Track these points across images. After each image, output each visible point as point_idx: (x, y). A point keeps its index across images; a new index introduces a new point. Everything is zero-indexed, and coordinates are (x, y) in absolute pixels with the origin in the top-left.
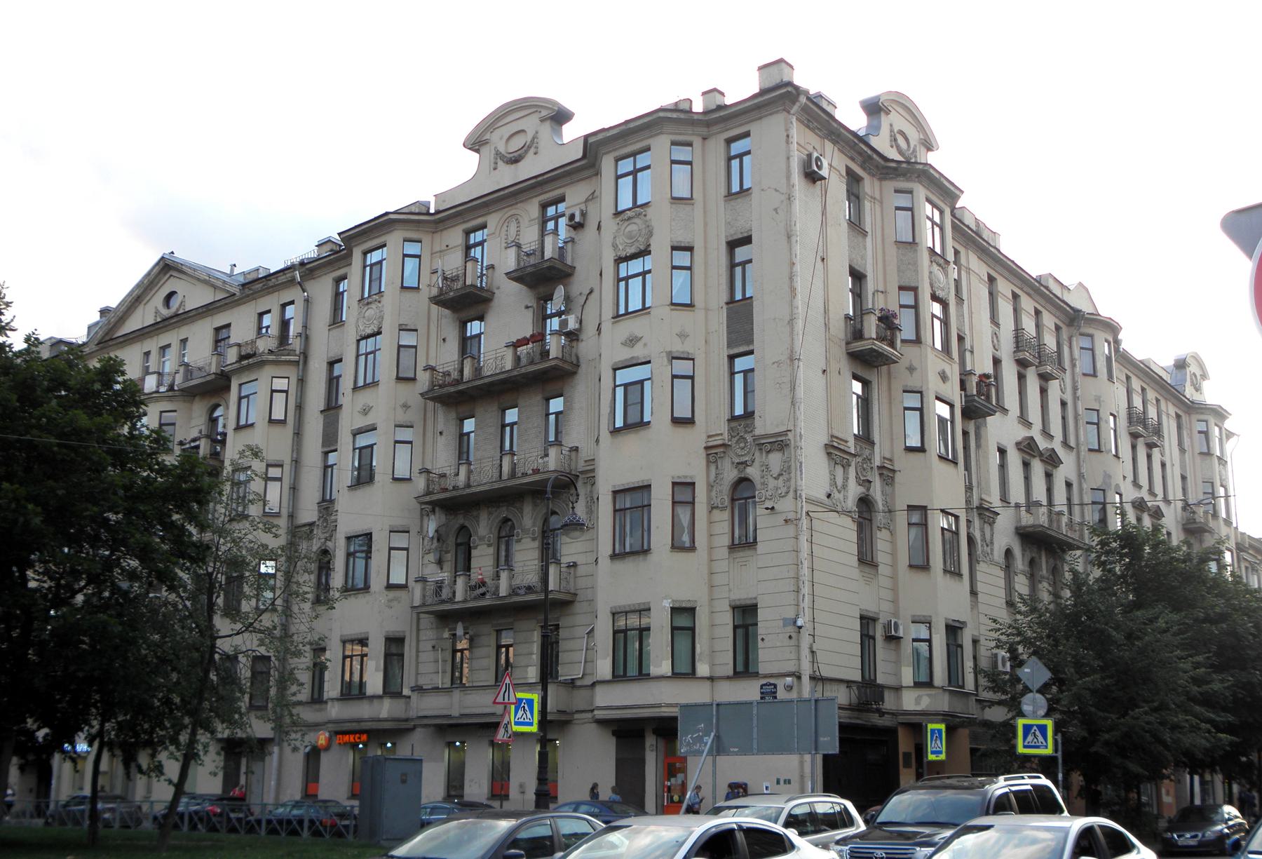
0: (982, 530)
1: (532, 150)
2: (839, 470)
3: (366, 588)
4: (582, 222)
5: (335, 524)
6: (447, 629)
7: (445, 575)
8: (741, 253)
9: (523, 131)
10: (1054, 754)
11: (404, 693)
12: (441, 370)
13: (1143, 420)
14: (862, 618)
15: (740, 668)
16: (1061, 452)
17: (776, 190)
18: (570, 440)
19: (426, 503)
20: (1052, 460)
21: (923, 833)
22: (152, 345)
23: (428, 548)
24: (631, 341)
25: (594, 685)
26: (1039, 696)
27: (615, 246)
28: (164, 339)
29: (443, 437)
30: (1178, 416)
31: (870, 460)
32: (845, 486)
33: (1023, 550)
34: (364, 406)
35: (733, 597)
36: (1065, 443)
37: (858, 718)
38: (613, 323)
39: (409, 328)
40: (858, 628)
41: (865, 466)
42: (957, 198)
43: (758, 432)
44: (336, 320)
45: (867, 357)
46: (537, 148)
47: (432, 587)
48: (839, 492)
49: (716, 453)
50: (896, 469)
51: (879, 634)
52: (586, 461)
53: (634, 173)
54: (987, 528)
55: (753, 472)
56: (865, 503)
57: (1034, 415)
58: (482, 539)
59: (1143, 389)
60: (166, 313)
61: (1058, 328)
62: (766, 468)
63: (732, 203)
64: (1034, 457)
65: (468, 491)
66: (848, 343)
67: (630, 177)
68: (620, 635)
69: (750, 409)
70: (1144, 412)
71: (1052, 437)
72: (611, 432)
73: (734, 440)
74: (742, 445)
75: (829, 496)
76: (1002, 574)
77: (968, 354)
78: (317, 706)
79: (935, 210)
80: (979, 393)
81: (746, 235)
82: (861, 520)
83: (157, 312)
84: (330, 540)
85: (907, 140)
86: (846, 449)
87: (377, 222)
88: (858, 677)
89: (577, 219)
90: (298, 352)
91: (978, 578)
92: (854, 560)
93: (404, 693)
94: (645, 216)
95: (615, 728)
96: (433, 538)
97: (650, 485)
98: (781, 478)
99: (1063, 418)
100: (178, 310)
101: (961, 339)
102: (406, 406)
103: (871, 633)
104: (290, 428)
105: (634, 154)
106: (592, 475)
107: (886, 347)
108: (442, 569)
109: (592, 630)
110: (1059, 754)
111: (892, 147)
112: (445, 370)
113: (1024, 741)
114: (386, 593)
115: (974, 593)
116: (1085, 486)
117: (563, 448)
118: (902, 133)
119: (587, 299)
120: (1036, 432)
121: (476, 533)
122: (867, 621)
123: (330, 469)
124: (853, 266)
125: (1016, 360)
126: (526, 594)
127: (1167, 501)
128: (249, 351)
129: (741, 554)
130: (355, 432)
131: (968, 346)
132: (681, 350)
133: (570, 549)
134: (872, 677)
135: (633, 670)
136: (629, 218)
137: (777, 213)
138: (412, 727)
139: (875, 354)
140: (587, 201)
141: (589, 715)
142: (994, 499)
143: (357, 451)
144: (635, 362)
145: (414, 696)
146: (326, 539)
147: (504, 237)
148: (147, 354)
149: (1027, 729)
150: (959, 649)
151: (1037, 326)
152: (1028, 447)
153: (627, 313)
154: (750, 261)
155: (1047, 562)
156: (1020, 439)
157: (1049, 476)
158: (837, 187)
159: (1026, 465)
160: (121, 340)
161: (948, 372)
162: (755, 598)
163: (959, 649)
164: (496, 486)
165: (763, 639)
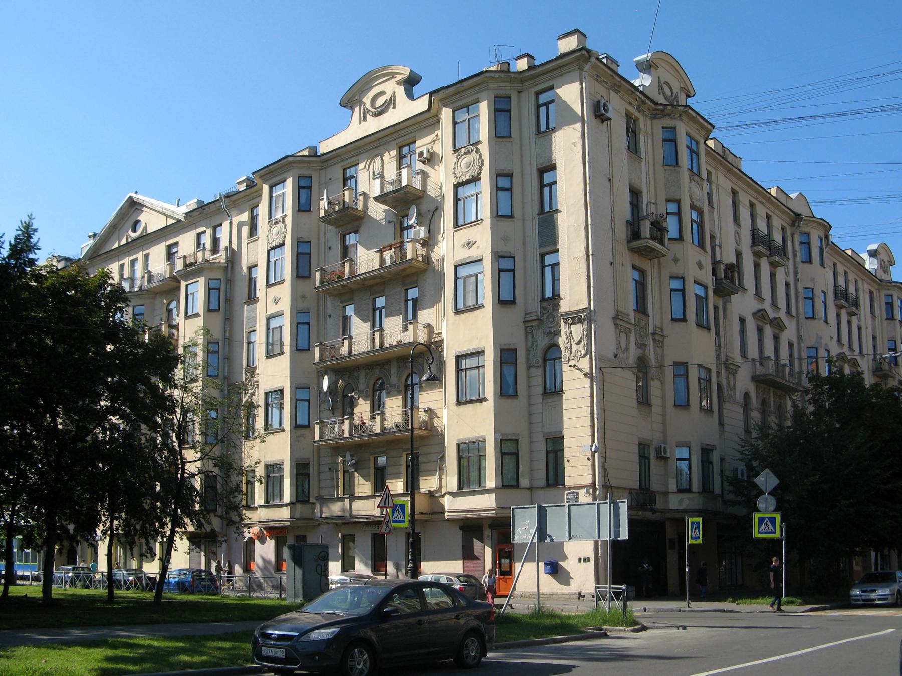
0: (727, 378)
2: (623, 337)
10: (780, 538)
14: (640, 444)
20: (778, 326)
32: (627, 349)
42: (709, 132)
48: (624, 353)
49: (532, 326)
57: (766, 293)
70: (846, 290)
74: (551, 320)
75: (616, 356)
76: (741, 410)
86: (628, 321)
95: (461, 525)
100: (142, 233)
103: (647, 455)
115: (721, 424)
116: (802, 345)
118: (667, 83)
134: (647, 487)
149: (761, 520)
152: (760, 315)
159: (760, 330)
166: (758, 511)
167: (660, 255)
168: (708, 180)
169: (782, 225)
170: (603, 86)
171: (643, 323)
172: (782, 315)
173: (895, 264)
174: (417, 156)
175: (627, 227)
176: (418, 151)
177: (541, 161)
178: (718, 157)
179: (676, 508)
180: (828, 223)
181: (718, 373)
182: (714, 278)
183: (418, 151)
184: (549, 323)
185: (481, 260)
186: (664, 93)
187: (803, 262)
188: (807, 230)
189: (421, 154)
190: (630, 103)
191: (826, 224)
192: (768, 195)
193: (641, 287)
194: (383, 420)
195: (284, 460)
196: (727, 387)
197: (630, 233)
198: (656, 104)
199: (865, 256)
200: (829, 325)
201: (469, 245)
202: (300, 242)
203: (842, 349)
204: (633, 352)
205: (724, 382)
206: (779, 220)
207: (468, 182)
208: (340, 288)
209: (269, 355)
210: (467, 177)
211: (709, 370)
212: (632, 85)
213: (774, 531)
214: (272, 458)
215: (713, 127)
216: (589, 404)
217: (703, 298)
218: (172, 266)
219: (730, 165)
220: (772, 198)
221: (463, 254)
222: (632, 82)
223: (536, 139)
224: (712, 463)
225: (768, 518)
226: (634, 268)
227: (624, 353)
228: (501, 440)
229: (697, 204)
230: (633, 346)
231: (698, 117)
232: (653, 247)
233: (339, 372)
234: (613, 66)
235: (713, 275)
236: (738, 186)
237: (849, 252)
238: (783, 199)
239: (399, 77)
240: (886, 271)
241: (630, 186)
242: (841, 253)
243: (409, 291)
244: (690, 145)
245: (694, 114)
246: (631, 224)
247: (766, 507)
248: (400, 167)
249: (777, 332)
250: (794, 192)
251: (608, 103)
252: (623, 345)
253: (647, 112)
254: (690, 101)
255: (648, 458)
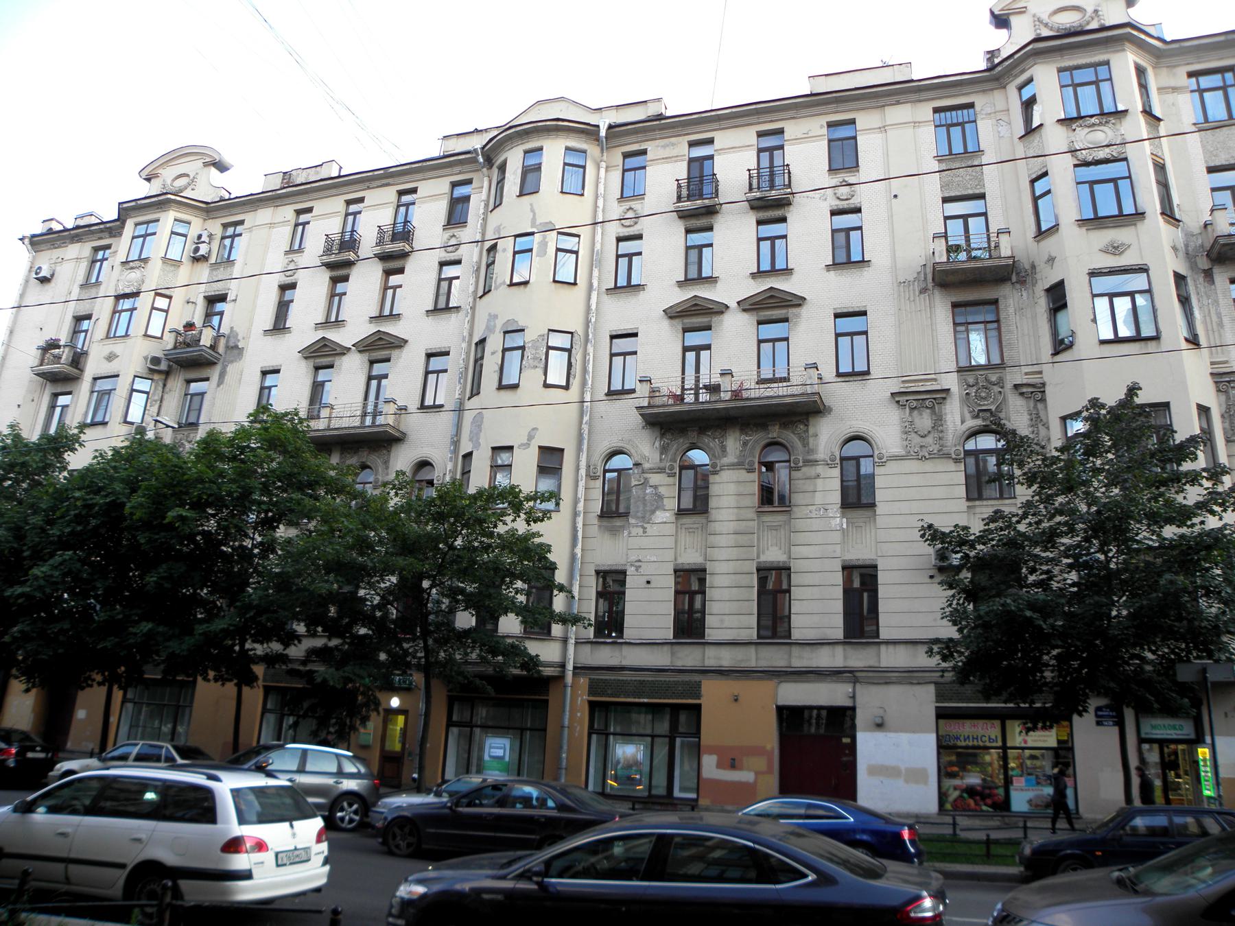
21: (710, 838)
24: (1116, 248)
53: (145, 236)
67: (142, 239)
87: (424, 164)
102: (1051, 260)
105: (148, 222)
136: (1094, 125)
143: (96, 394)
153: (114, 337)
154: (400, 286)
164: (358, 431)
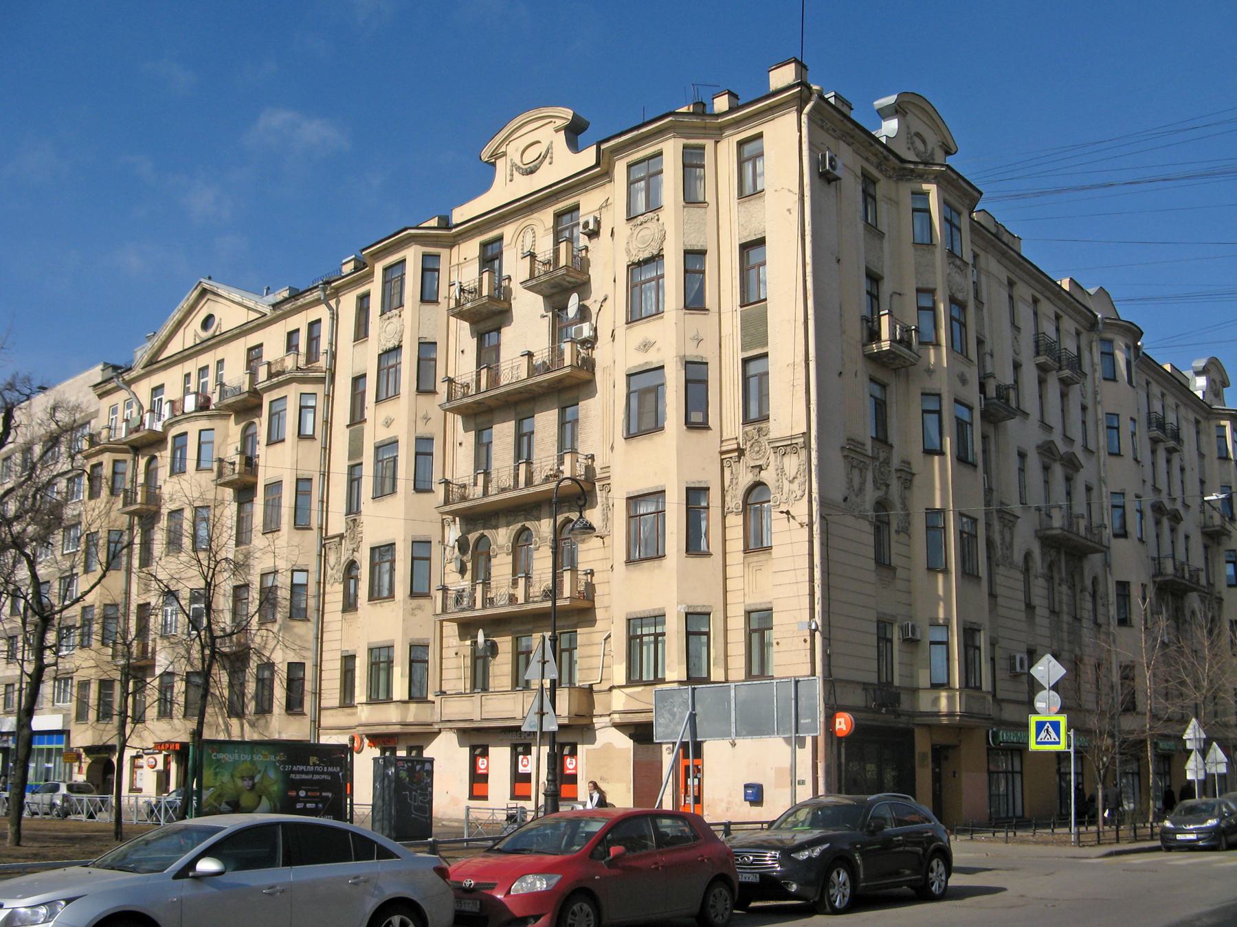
0: (1002, 533)
1: (548, 160)
2: (856, 472)
3: (391, 596)
4: (596, 229)
5: (360, 535)
6: (469, 637)
7: (466, 583)
8: (754, 254)
9: (538, 142)
10: (1067, 750)
11: (429, 699)
12: (459, 382)
13: (1161, 425)
14: (879, 622)
15: (755, 671)
16: (1081, 456)
17: (789, 190)
18: (584, 448)
19: (447, 513)
20: (1071, 464)
22: (192, 366)
23: (449, 557)
25: (611, 689)
26: (1052, 693)
27: (628, 252)
28: (203, 360)
29: (463, 448)
30: (1197, 422)
31: (888, 463)
32: (861, 490)
33: (1043, 555)
34: (386, 419)
35: (748, 601)
36: (1085, 448)
37: (874, 720)
38: (627, 329)
39: (427, 340)
40: (875, 631)
41: (882, 469)
42: (975, 201)
43: (772, 435)
44: (361, 332)
45: (885, 360)
46: (552, 158)
47: (454, 596)
48: (857, 496)
49: (731, 458)
50: (914, 471)
51: (896, 635)
52: (601, 469)
54: (1006, 531)
55: (767, 476)
56: (882, 505)
57: (1054, 418)
58: (501, 547)
59: (1163, 395)
60: (205, 335)
61: (1078, 334)
62: (781, 471)
63: (747, 205)
64: (1055, 461)
65: (486, 500)
66: (864, 345)
68: (633, 641)
69: (764, 413)
70: (1164, 418)
71: (1051, 428)
72: (625, 439)
73: (749, 444)
74: (756, 449)
75: (845, 499)
76: (1021, 577)
77: (988, 358)
78: (348, 710)
79: (953, 213)
80: (999, 397)
81: (759, 236)
82: (878, 524)
83: (196, 335)
84: (357, 551)
85: (924, 142)
86: (864, 451)
88: (873, 678)
89: (591, 226)
90: (324, 369)
91: (998, 582)
92: (871, 564)
93: (429, 699)
94: (658, 220)
95: (632, 732)
96: (454, 547)
97: (664, 491)
98: (796, 481)
99: (1084, 422)
100: (215, 332)
101: (980, 342)
103: (889, 636)
104: (317, 444)
106: (608, 482)
107: (902, 348)
108: (463, 577)
109: (609, 636)
110: (1072, 750)
111: (909, 149)
112: (463, 381)
113: (1037, 738)
114: (410, 601)
115: (992, 596)
116: (1104, 489)
117: (579, 456)
118: (918, 135)
119: (601, 306)
120: (1057, 437)
121: (496, 542)
122: (883, 625)
123: (356, 482)
124: (871, 267)
125: (1037, 364)
126: (543, 601)
127: (1186, 506)
128: (279, 368)
129: (756, 559)
130: (377, 445)
131: (987, 348)
132: (696, 354)
133: (589, 554)
134: (889, 679)
135: (382, 696)
137: (790, 213)
138: (437, 730)
139: (892, 356)
140: (600, 209)
141: (607, 719)
142: (1016, 507)
144: (648, 367)
145: (437, 700)
146: (354, 551)
147: (521, 247)
148: (188, 376)
149: (1040, 726)
150: (977, 651)
151: (1058, 330)
152: (1047, 450)
155: (1067, 566)
156: (1040, 442)
157: (1068, 479)
158: (852, 187)
159: (1046, 468)
160: (164, 362)
161: (968, 376)
162: (771, 603)
163: (977, 651)
165: (778, 643)
166: (1036, 712)
167: (908, 363)
168: (974, 266)
169: (1076, 329)
170: (831, 135)
171: (882, 456)
172: (1078, 450)
173: (1228, 386)
174: (581, 227)
175: (862, 324)
176: (582, 221)
177: (746, 234)
178: (989, 235)
179: (929, 710)
180: (1138, 328)
181: (988, 525)
182: (982, 396)
183: (582, 221)
184: (754, 454)
185: (663, 367)
186: (915, 149)
187: (1105, 379)
188: (1108, 335)
189: (586, 224)
190: (867, 159)
191: (1136, 329)
192: (1058, 289)
193: (880, 407)
194: (528, 585)
195: (393, 640)
196: (1002, 544)
197: (865, 332)
198: (903, 161)
199: (1189, 373)
200: (1141, 464)
201: (646, 346)
202: (423, 343)
203: (1174, 504)
204: (871, 495)
205: (997, 538)
206: (1072, 321)
207: (647, 261)
208: (475, 406)
209: (279, 484)
210: (647, 255)
211: (974, 521)
212: (873, 137)
213: (1057, 740)
214: (379, 638)
215: (981, 194)
216: (807, 565)
217: (967, 423)
218: (253, 374)
219: (1004, 247)
220: (1063, 293)
221: (638, 360)
222: (873, 133)
223: (739, 204)
224: (979, 648)
225: (1050, 722)
226: (872, 380)
227: (857, 496)
228: (687, 614)
229: (960, 296)
230: (869, 485)
231: (960, 180)
232: (898, 352)
233: (471, 519)
234: (845, 109)
235: (980, 393)
236: (1017, 276)
237: (1168, 367)
238: (1079, 296)
239: (559, 123)
240: (1218, 395)
241: (867, 268)
242: (1155, 368)
243: (568, 409)
244: (949, 218)
245: (955, 177)
246: (868, 321)
247: (1047, 706)
248: (557, 243)
249: (1070, 471)
250: (1092, 286)
251: (836, 158)
252: (856, 485)
253: (891, 173)
254: (950, 160)
255: (891, 641)
